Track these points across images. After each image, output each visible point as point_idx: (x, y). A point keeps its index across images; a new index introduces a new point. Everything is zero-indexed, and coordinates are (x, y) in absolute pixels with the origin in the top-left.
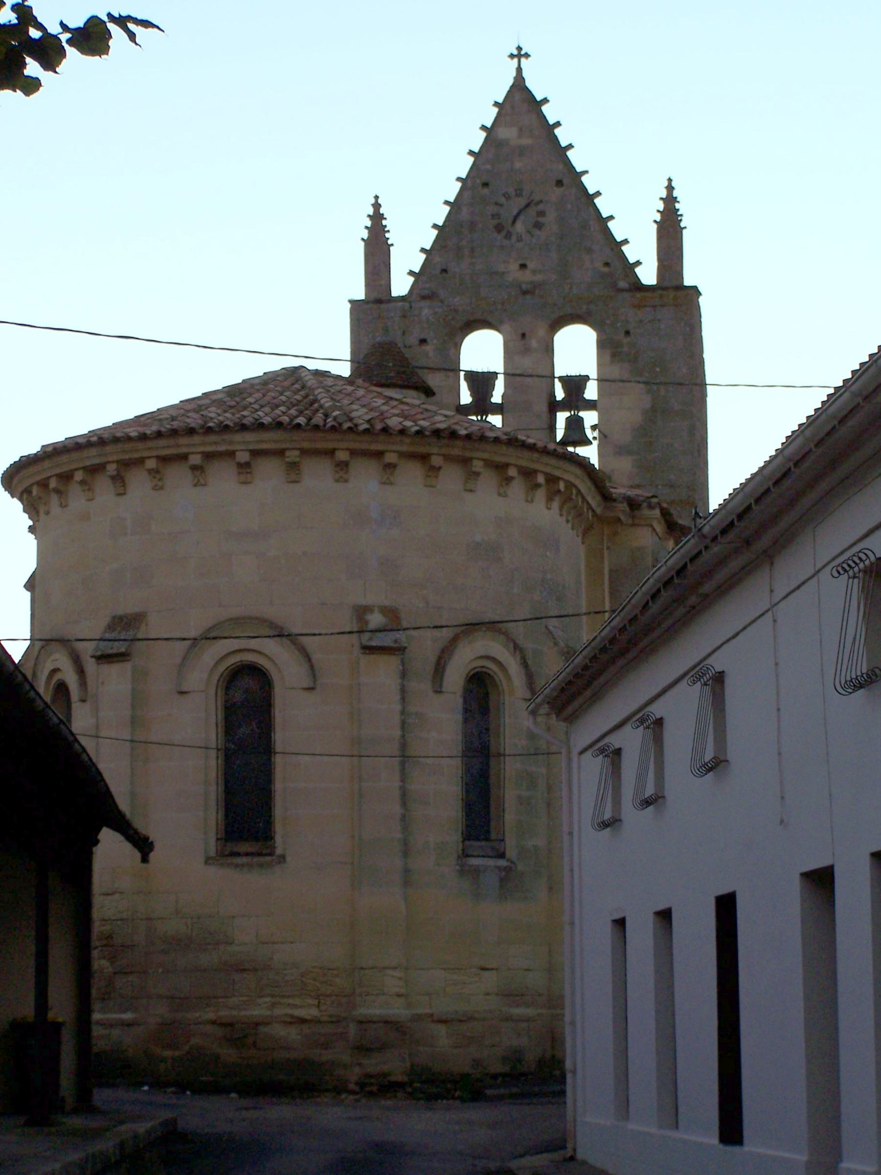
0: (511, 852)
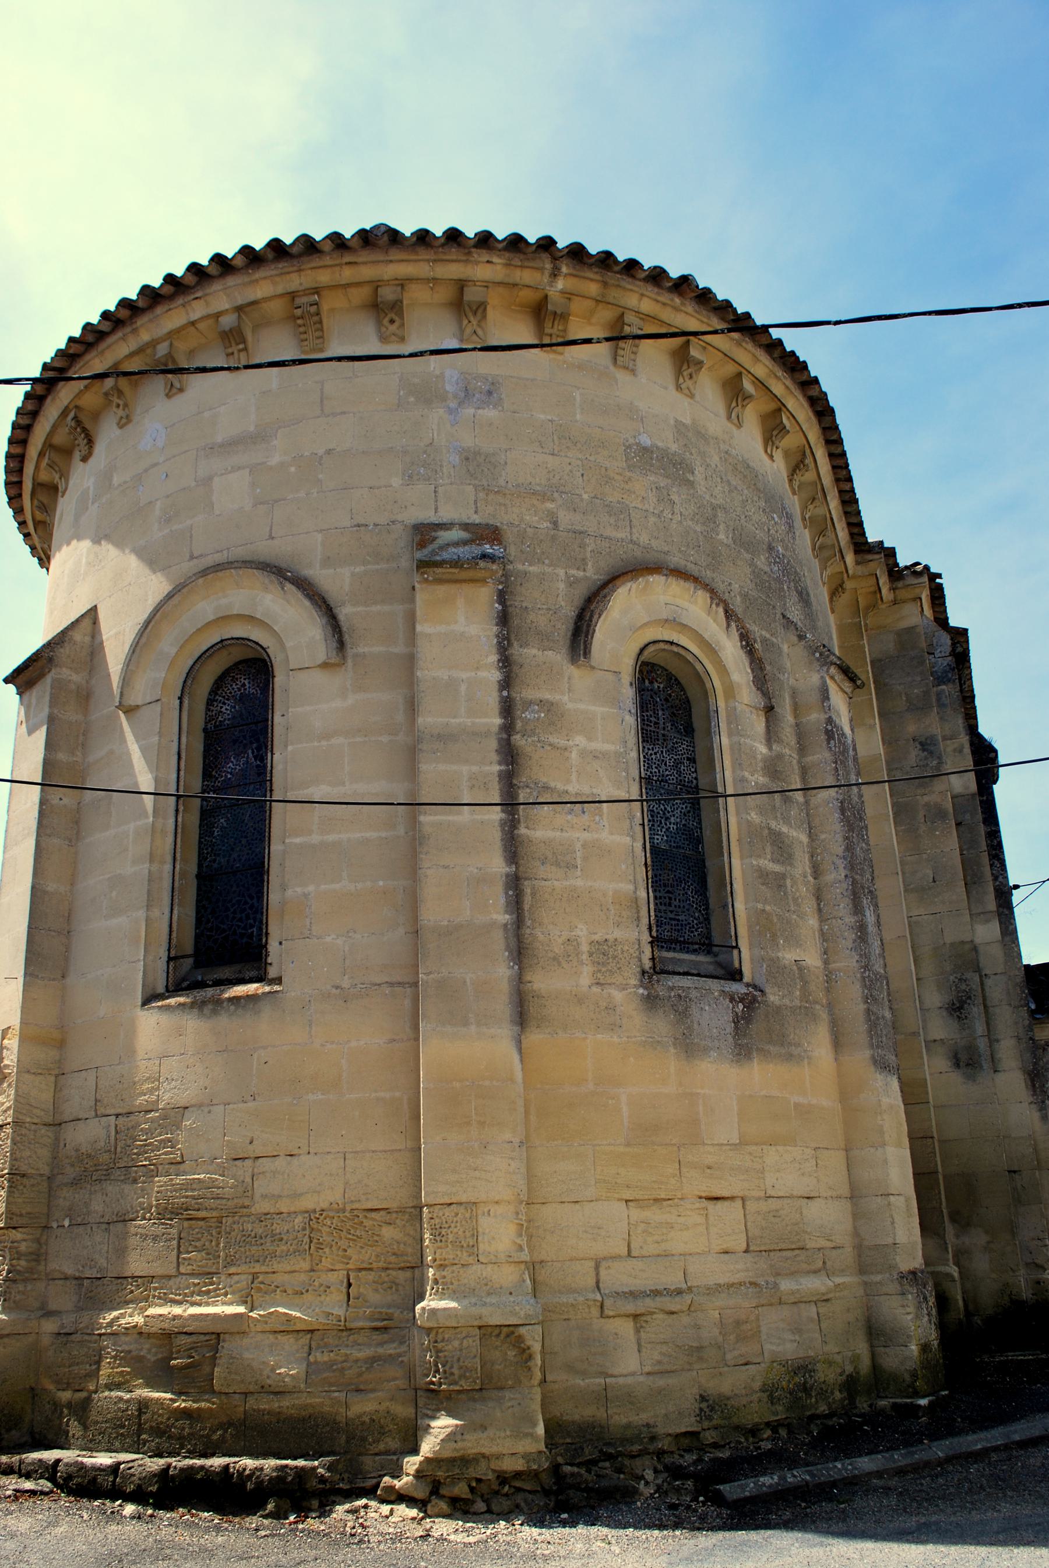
0: (747, 959)
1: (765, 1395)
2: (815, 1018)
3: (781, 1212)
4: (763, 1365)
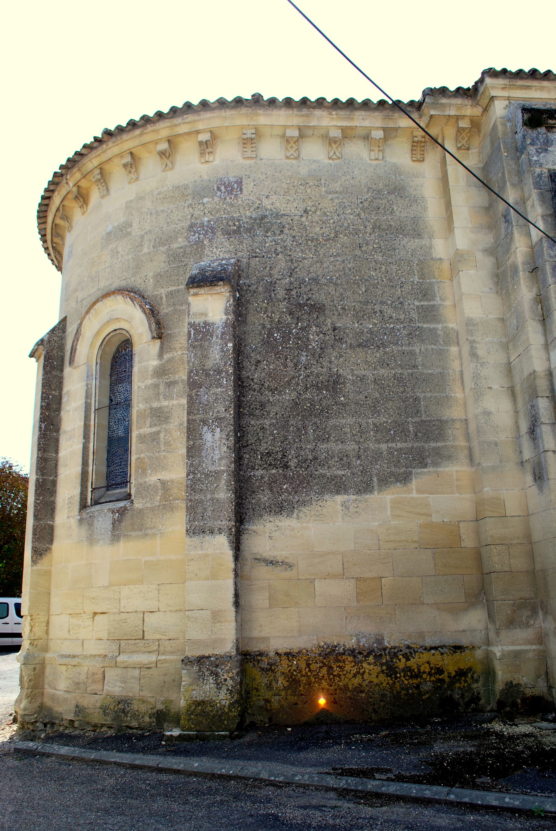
1: (102, 710)
2: (172, 509)
3: (128, 620)
4: (102, 696)
